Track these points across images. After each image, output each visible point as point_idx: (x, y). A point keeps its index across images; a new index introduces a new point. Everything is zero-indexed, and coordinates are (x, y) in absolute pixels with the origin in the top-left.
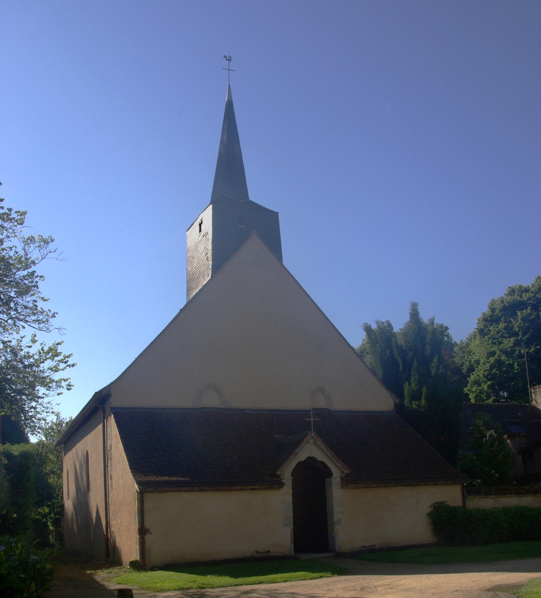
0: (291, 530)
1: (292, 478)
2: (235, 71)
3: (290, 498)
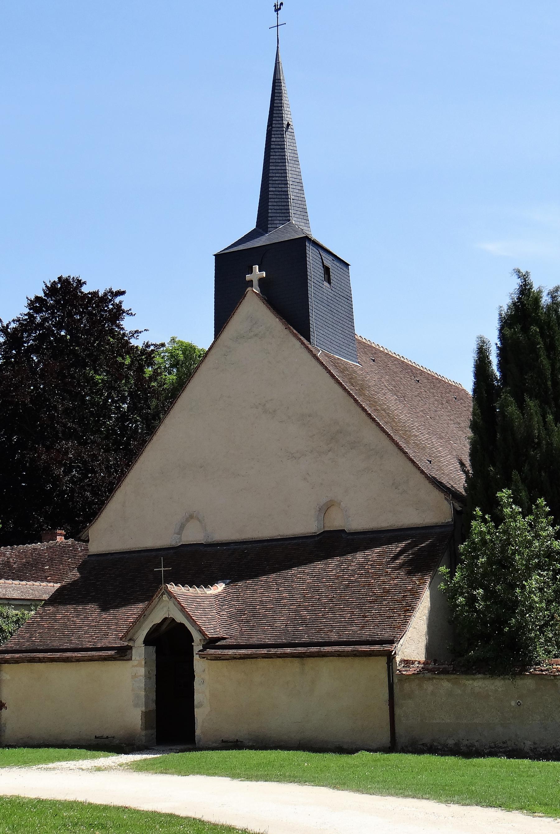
0: (142, 712)
1: (193, 644)
2: (285, 24)
3: (142, 671)
